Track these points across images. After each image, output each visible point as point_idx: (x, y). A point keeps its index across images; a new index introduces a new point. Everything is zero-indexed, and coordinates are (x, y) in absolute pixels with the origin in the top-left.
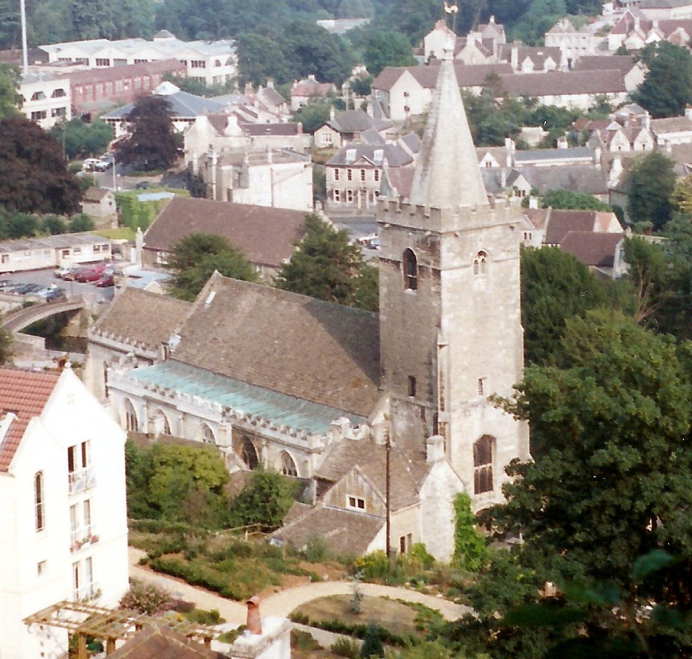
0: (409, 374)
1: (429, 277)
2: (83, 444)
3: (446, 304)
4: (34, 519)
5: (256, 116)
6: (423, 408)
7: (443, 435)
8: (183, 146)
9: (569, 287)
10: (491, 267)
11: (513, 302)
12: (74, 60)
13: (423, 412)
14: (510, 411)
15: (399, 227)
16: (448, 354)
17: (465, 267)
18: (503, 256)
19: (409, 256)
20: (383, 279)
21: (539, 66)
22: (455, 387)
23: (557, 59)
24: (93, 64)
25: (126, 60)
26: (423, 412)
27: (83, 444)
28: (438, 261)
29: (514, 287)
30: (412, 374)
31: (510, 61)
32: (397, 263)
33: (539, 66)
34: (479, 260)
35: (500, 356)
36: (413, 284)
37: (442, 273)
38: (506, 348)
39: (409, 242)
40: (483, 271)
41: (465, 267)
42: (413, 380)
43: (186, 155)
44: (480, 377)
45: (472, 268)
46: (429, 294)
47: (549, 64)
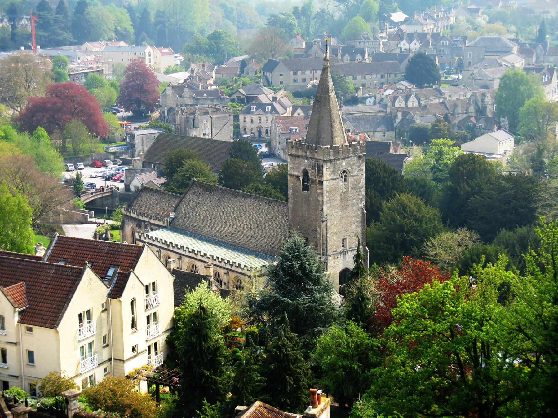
2: (154, 284)
3: (325, 199)
4: (131, 323)
7: (183, 158)
9: (231, 103)
10: (350, 179)
11: (361, 197)
15: (298, 156)
16: (326, 225)
17: (336, 179)
19: (305, 173)
21: (353, 59)
22: (330, 243)
27: (154, 284)
28: (321, 177)
29: (361, 190)
31: (337, 56)
32: (298, 177)
33: (353, 59)
34: (343, 176)
35: (354, 226)
37: (324, 183)
38: (357, 222)
40: (346, 181)
41: (336, 179)
44: (343, 238)
45: (339, 180)
46: (316, 193)
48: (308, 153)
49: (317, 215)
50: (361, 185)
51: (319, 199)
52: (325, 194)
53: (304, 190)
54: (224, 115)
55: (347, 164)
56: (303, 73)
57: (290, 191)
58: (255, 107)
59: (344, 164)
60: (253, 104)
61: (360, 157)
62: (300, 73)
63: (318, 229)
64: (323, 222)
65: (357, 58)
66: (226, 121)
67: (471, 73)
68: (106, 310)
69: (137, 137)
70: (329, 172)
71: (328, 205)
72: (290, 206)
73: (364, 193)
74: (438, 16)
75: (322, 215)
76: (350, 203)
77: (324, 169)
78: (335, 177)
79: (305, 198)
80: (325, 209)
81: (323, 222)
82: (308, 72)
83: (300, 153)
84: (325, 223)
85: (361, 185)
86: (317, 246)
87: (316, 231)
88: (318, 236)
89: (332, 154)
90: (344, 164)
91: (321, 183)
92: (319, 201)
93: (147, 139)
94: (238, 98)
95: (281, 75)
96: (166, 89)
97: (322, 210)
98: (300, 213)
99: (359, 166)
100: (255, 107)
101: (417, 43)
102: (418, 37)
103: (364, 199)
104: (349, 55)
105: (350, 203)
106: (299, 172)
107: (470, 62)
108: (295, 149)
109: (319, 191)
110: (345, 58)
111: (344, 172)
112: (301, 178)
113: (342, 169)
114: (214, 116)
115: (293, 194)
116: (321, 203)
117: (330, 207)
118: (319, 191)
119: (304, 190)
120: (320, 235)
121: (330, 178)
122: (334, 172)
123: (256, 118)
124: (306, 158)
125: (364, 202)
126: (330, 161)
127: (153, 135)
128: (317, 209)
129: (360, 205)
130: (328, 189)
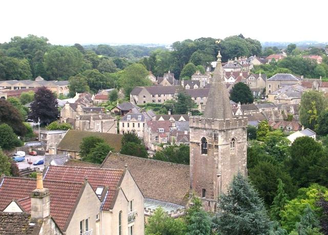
0: (203, 188)
1: (213, 148)
5: (85, 106)
6: (209, 202)
8: (60, 115)
10: (236, 145)
11: (244, 159)
12: (5, 87)
13: (209, 203)
14: (174, 232)
15: (199, 128)
18: (241, 141)
19: (204, 140)
20: (191, 150)
23: (199, 85)
24: (13, 89)
25: (25, 87)
26: (209, 203)
29: (245, 153)
30: (205, 188)
32: (198, 144)
34: (232, 142)
36: (204, 151)
39: (204, 134)
40: (234, 147)
42: (204, 191)
43: (61, 119)
45: (230, 145)
46: (213, 155)
47: (196, 86)
48: (207, 126)
49: (213, 172)
50: (244, 150)
51: (215, 159)
52: (220, 155)
53: (203, 153)
54: (111, 120)
55: (236, 133)
56: (159, 96)
57: (191, 155)
58: (130, 116)
59: (233, 133)
60: (129, 114)
61: (244, 129)
62: (157, 96)
63: (214, 182)
64: (218, 176)
65: (194, 87)
66: (112, 124)
67: (274, 96)
68: (99, 220)
69: (48, 136)
70: (223, 139)
71: (222, 164)
72: (191, 165)
73: (246, 156)
74: (243, 63)
75: (217, 171)
76: (237, 163)
77: (219, 137)
78: (227, 143)
79: (204, 159)
80: (220, 166)
81: (218, 176)
82: (162, 95)
83: (200, 125)
84: (220, 177)
85: (244, 150)
86: (213, 195)
87: (213, 183)
88: (214, 187)
89: (225, 125)
90: (233, 133)
91: (217, 147)
92: (215, 161)
93: (55, 137)
94: (116, 112)
95: (144, 97)
96: (65, 105)
97: (217, 168)
98: (199, 172)
99: (243, 135)
100: (130, 116)
101: (233, 79)
102: (233, 74)
103: (246, 160)
104: (189, 85)
105: (237, 163)
106: (199, 140)
107: (270, 91)
108: (195, 123)
109: (215, 153)
110: (186, 87)
111: (233, 139)
112: (200, 144)
113: (232, 137)
114: (104, 121)
115: (194, 157)
116: (216, 162)
117: (223, 165)
118: (215, 153)
119: (203, 153)
120: (216, 187)
121: (224, 143)
122: (226, 139)
123: (131, 124)
124: (205, 129)
125: (246, 163)
126: (224, 131)
127: (60, 135)
128: (213, 167)
129: (244, 165)
130: (222, 152)
